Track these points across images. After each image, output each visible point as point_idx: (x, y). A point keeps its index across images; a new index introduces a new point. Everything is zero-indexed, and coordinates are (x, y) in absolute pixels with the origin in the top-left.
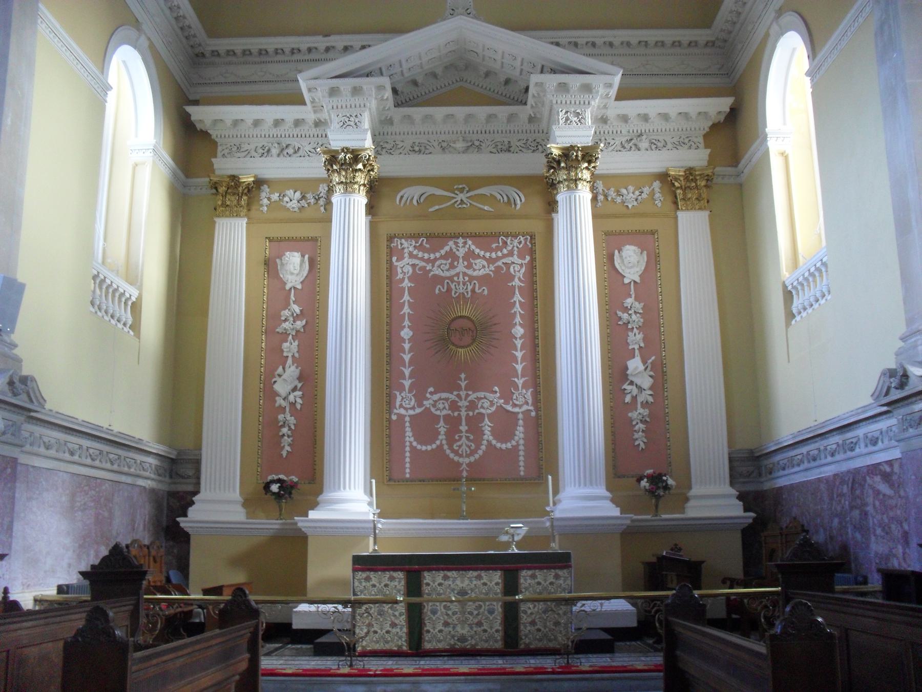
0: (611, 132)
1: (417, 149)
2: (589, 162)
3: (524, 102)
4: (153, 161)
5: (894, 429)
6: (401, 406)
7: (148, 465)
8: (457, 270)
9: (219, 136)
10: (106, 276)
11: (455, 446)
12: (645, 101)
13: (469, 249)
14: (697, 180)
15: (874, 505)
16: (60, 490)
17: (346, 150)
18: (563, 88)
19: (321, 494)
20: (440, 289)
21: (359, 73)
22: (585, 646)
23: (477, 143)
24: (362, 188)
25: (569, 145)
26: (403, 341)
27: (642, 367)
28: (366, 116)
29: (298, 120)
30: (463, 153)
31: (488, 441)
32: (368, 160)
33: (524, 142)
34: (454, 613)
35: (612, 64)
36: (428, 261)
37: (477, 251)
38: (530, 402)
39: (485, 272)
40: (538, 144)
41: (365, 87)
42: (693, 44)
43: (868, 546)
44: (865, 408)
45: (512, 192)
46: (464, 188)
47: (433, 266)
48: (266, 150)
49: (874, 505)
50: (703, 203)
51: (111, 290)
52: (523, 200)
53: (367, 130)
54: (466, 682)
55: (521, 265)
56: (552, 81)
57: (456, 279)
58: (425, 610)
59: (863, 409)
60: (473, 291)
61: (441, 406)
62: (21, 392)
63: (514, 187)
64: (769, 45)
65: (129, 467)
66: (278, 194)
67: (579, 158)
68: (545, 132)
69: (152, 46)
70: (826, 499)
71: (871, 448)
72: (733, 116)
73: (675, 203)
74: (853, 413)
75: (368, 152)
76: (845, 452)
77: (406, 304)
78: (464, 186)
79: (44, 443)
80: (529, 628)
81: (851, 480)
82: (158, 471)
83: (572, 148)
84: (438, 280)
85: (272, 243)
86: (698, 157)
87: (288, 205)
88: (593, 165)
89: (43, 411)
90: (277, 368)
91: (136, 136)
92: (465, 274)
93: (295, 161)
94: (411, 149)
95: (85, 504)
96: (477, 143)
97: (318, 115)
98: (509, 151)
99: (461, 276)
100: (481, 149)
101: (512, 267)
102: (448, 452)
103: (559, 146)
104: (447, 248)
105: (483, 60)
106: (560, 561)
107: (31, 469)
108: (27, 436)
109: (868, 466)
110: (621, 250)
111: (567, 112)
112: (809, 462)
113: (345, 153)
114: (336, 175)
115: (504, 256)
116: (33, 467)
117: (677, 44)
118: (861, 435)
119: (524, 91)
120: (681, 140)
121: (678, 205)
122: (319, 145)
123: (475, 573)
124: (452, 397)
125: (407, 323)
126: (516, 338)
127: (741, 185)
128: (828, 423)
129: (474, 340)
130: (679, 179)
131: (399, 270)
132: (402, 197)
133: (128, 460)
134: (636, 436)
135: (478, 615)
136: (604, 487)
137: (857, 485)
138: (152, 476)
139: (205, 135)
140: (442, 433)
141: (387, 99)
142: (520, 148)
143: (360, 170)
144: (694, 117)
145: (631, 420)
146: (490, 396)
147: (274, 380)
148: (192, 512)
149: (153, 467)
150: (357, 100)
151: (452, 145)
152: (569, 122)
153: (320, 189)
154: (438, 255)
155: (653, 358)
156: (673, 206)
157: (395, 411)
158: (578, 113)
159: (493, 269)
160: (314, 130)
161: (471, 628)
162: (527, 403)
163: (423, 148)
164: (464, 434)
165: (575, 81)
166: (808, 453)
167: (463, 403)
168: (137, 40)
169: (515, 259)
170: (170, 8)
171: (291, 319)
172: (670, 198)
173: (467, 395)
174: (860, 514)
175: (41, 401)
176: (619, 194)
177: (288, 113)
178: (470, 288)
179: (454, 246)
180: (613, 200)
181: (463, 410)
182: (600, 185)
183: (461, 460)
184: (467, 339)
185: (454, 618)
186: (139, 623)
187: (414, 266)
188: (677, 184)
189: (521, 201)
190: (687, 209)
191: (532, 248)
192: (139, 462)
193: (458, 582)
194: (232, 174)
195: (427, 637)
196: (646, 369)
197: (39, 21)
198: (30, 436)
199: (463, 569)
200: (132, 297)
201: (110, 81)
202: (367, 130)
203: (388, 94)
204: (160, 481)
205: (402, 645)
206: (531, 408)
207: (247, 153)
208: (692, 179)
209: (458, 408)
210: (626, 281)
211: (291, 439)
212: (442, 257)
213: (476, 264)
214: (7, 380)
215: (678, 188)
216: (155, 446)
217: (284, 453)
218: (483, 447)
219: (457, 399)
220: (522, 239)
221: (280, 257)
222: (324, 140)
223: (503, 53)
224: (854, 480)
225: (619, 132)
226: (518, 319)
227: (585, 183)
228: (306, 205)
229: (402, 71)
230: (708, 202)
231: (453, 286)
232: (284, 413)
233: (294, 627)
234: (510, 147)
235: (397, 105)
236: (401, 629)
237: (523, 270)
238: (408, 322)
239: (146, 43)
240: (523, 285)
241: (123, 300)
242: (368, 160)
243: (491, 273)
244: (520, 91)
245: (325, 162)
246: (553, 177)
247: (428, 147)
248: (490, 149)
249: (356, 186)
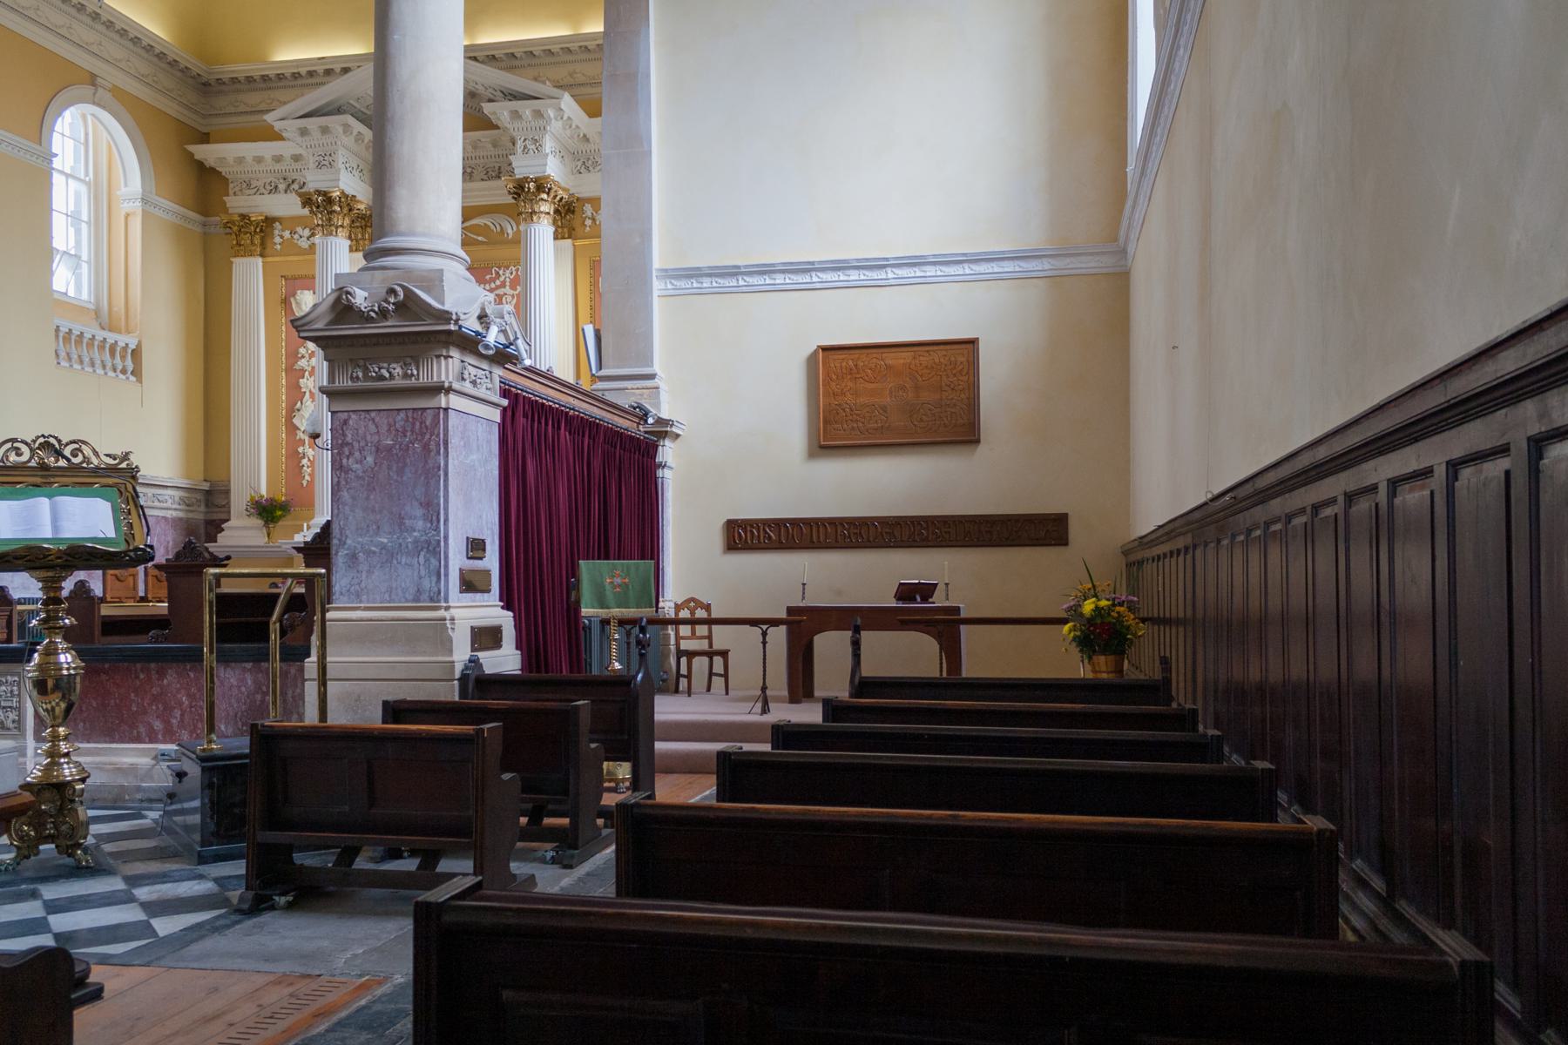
17: (319, 192)
18: (516, 115)
21: (324, 111)
55: (513, 297)
63: (505, 214)
69: (117, 93)
85: (288, 281)
90: (296, 404)
91: (126, 185)
101: (504, 298)
111: (525, 140)
165: (526, 108)
169: (507, 290)
171: (307, 356)
204: (187, 511)
217: (305, 483)
220: (514, 269)
221: (294, 295)
232: (303, 445)
234: (500, 173)
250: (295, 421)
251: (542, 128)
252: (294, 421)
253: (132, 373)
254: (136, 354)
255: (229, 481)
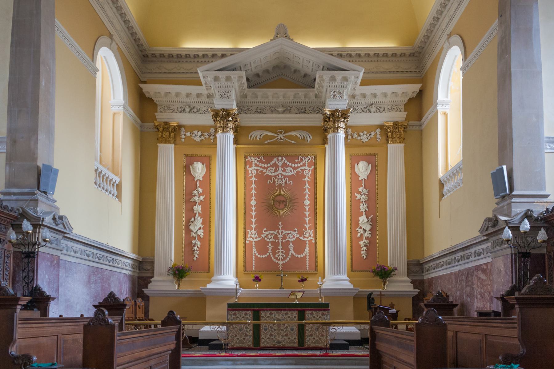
0: (356, 103)
1: (259, 111)
2: (345, 118)
3: (313, 87)
4: (124, 112)
5: (489, 248)
6: (251, 237)
7: (128, 264)
8: (278, 173)
9: (158, 101)
10: (102, 170)
11: (276, 255)
12: (374, 86)
13: (284, 162)
14: (399, 128)
15: (477, 285)
16: (83, 273)
17: (223, 110)
18: (333, 78)
19: (213, 277)
20: (269, 182)
21: (229, 69)
22: (334, 347)
23: (289, 108)
24: (231, 130)
25: (335, 109)
26: (252, 206)
27: (366, 220)
28: (233, 92)
29: (198, 93)
30: (282, 113)
31: (291, 253)
32: (234, 115)
33: (313, 108)
34: (275, 330)
35: (360, 65)
36: (264, 168)
37: (288, 163)
38: (312, 236)
39: (292, 174)
40: (319, 109)
41: (232, 76)
42: (403, 55)
43: (473, 304)
44: (476, 238)
45: (305, 134)
46: (282, 132)
47: (266, 171)
48: (183, 109)
49: (477, 285)
50: (402, 140)
51: (105, 178)
52: (311, 138)
53: (234, 100)
54: (279, 360)
56: (328, 74)
57: (277, 177)
58: (261, 329)
59: (475, 238)
60: (286, 183)
61: (270, 237)
62: (59, 223)
64: (443, 54)
65: (118, 264)
66: (190, 133)
67: (340, 116)
68: (323, 103)
69: (119, 48)
70: (454, 282)
71: (478, 258)
72: (421, 93)
73: (387, 140)
74: (469, 240)
75: (234, 111)
76: (465, 260)
77: (253, 188)
78: (282, 130)
79: (73, 250)
80: (309, 337)
81: (467, 273)
82: (133, 266)
83: (337, 110)
84: (270, 177)
86: (400, 116)
87: (195, 138)
88: (346, 120)
89: (72, 234)
91: (114, 98)
92: (282, 175)
93: (198, 115)
94: (256, 111)
95: (96, 280)
96: (289, 108)
97: (209, 91)
98: (305, 113)
99: (280, 175)
100: (291, 111)
102: (273, 258)
103: (330, 110)
104: (273, 162)
105: (293, 63)
106: (325, 307)
107: (67, 263)
108: (64, 246)
109: (475, 266)
110: (359, 163)
111: (334, 92)
112: (447, 265)
113: (222, 111)
114: (218, 123)
115: (301, 166)
116: (68, 261)
117: (394, 55)
118: (473, 252)
119: (313, 80)
120: (393, 107)
121: (388, 141)
122: (210, 107)
123: (285, 312)
124: (275, 233)
125: (254, 198)
126: (306, 206)
127: (422, 130)
128: (456, 246)
129: (286, 206)
130: (390, 128)
131: (250, 172)
132: (251, 136)
133: (117, 261)
134: (362, 252)
135: (286, 331)
136: (346, 275)
137: (469, 276)
138: (130, 269)
139: (150, 100)
140: (270, 249)
141: (244, 83)
142: (311, 111)
143: (230, 120)
144: (400, 95)
145: (360, 245)
146: (293, 233)
147: (189, 224)
148: (150, 286)
149: (130, 265)
150: (228, 83)
151: (277, 109)
152: (335, 97)
153: (211, 130)
154: (269, 165)
155: (372, 216)
156: (386, 141)
157: (248, 239)
158: (340, 92)
159: (296, 172)
160: (207, 99)
161: (283, 337)
162: (311, 236)
163: (262, 110)
164: (280, 250)
165: (339, 75)
166: (446, 261)
167: (280, 236)
168: (111, 44)
169: (306, 167)
170: (128, 28)
171: (198, 195)
172: (384, 138)
173: (282, 232)
174: (470, 289)
175: (71, 229)
176: (359, 135)
177: (193, 89)
178: (284, 181)
179: (277, 161)
180: (356, 138)
181: (280, 239)
182: (349, 130)
183: (279, 262)
184: (282, 206)
185: (275, 332)
186: (13, 338)
187: (257, 170)
188: (389, 130)
189: (310, 138)
190: (393, 143)
191: (315, 162)
192: (123, 262)
193: (277, 316)
194: (166, 121)
195: (262, 341)
196: (368, 221)
197: (56, 29)
198: (66, 246)
199: (280, 310)
200: (116, 182)
201: (97, 66)
202: (234, 100)
203: (244, 80)
205: (250, 345)
206: (313, 239)
207: (173, 110)
208: (397, 128)
209: (278, 238)
210: (360, 179)
211: (198, 252)
212: (271, 166)
213: (287, 170)
214: (52, 217)
215: (389, 132)
216: (132, 255)
217: (195, 259)
218: (290, 256)
219: (277, 234)
221: (192, 164)
222: (212, 105)
223: (303, 59)
224: (468, 273)
225: (361, 103)
226: (307, 197)
227: (342, 129)
228: (204, 139)
229: (251, 68)
230: (404, 139)
231: (276, 180)
232: (195, 239)
233: (200, 338)
234: (305, 111)
235: (249, 87)
236: (250, 337)
237: (310, 173)
238: (254, 197)
239: (116, 47)
240: (310, 180)
241: (112, 183)
242: (234, 115)
243: (295, 174)
244: (312, 81)
245: (213, 116)
246: (326, 126)
247: (264, 110)
248: (296, 111)
249: (228, 129)
250: (191, 227)
251: (345, 86)
252: (190, 227)
253: (116, 197)
254: (119, 187)
255: (154, 257)
